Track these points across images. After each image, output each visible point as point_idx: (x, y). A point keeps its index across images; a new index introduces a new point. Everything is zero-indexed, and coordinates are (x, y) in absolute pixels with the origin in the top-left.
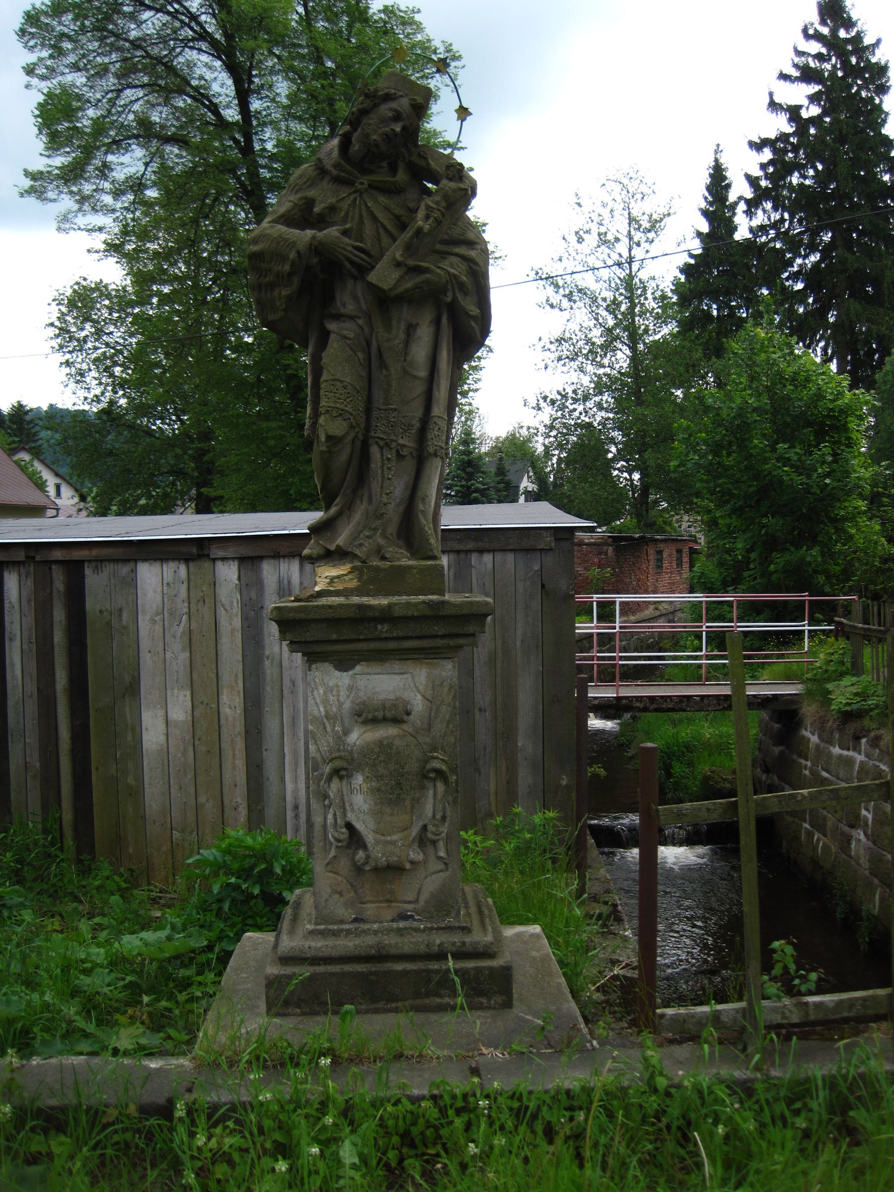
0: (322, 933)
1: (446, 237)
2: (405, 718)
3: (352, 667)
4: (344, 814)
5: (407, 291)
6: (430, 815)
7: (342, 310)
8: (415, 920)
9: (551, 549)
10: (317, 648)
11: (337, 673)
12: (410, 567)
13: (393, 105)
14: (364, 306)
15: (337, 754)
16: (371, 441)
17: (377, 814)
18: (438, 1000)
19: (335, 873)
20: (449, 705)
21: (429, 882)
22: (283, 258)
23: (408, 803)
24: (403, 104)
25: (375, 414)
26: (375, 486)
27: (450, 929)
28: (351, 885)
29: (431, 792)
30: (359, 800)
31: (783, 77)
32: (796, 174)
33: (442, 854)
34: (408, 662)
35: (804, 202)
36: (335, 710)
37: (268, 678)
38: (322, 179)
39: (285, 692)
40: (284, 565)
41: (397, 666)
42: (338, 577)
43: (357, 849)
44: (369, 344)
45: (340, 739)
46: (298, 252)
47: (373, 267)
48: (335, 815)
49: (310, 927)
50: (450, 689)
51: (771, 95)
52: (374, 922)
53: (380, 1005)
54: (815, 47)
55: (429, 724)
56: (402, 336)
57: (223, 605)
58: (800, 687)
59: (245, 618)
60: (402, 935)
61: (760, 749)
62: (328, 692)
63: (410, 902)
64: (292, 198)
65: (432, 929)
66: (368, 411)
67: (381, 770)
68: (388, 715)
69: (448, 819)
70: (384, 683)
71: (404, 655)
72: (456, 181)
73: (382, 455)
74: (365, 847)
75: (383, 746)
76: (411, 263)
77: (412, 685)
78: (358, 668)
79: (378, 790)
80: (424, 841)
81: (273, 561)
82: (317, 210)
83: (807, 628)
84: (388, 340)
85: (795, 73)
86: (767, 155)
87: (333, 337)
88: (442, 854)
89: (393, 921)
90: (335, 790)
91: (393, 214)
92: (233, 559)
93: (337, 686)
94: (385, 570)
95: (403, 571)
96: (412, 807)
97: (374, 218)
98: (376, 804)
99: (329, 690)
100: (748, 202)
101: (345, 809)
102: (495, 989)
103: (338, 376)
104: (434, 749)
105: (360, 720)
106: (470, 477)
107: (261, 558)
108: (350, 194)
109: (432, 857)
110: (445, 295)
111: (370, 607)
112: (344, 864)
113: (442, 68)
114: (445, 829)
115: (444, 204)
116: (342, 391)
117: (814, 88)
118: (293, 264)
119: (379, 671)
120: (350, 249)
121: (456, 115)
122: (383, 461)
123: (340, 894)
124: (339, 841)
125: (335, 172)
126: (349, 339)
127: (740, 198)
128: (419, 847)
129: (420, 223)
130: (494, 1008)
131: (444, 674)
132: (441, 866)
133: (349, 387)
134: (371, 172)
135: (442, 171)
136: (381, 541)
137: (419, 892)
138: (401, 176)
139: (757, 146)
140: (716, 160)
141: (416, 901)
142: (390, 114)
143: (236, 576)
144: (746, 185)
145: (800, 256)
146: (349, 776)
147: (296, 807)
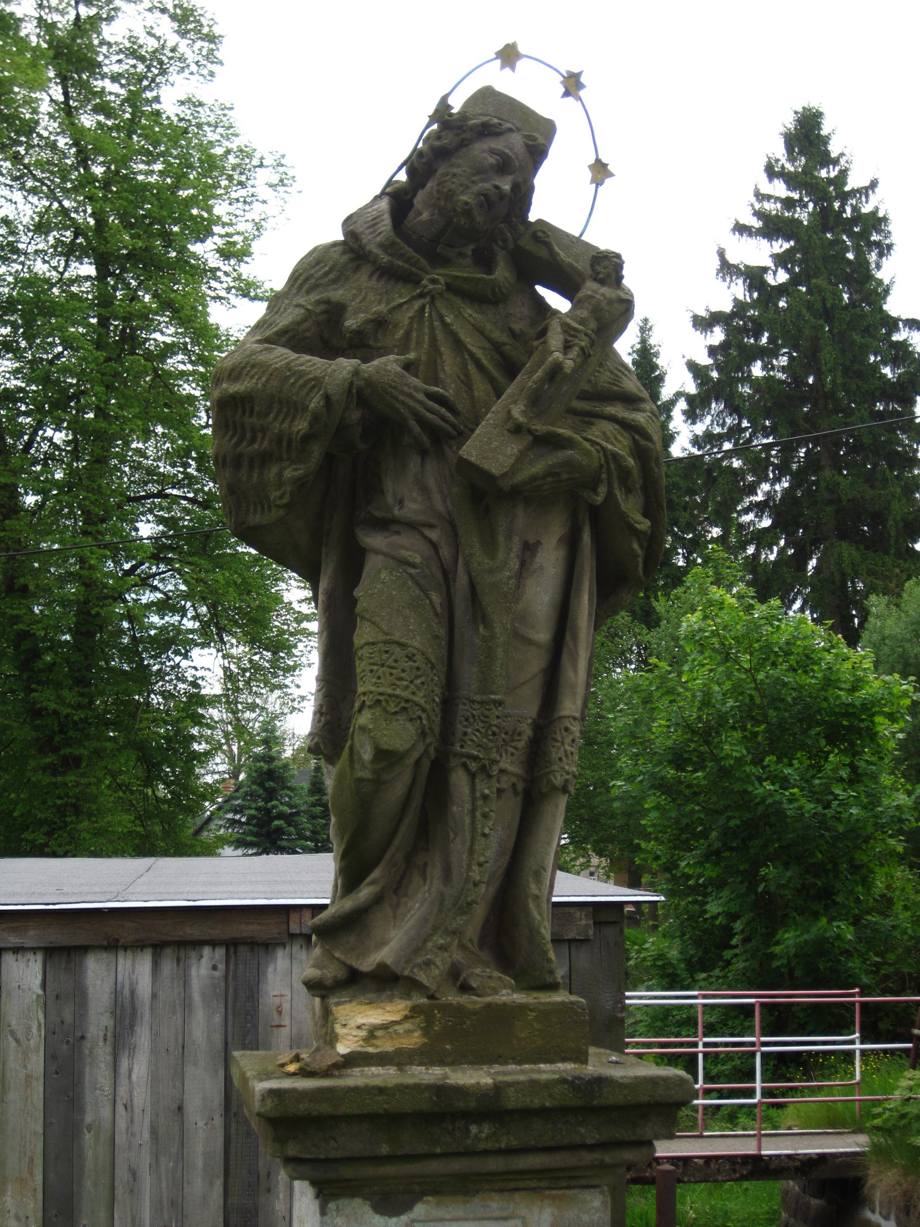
1: (587, 387)
3: (406, 1207)
5: (534, 478)
7: (396, 512)
9: (586, 941)
10: (346, 1172)
11: (378, 1220)
12: (523, 1008)
13: (498, 144)
14: (439, 505)
16: (454, 762)
22: (294, 408)
24: (515, 143)
25: (462, 709)
26: (459, 847)
31: (741, 229)
32: (759, 364)
34: (517, 1196)
35: (774, 404)
37: (89, 1165)
38: (357, 269)
39: (119, 1191)
40: (124, 962)
41: (495, 1204)
42: (385, 1027)
44: (448, 576)
46: (327, 398)
47: (473, 431)
51: (721, 254)
54: (780, 189)
56: (515, 564)
57: (12, 1033)
58: (863, 1139)
59: (51, 1056)
64: (302, 301)
66: (448, 704)
72: (610, 286)
73: (473, 790)
76: (540, 428)
78: (420, 1209)
81: (105, 955)
82: (351, 323)
83: (858, 1046)
84: (491, 571)
85: (756, 223)
86: (718, 336)
87: (373, 563)
91: (489, 340)
92: (34, 950)
94: (475, 1013)
95: (505, 1015)
97: (458, 345)
100: (690, 399)
103: (397, 636)
106: (271, 795)
107: (84, 949)
108: (414, 298)
110: (595, 490)
111: (460, 1091)
113: (572, 90)
115: (593, 325)
116: (408, 665)
117: (781, 246)
118: (316, 418)
119: (460, 1214)
120: (421, 397)
121: (589, 175)
122: (474, 800)
125: (385, 258)
126: (413, 566)
127: (679, 395)
129: (558, 355)
133: (418, 657)
134: (445, 262)
135: (583, 266)
136: (458, 956)
138: (502, 273)
139: (703, 323)
140: (643, 341)
142: (492, 160)
143: (38, 981)
144: (689, 377)
145: (766, 480)
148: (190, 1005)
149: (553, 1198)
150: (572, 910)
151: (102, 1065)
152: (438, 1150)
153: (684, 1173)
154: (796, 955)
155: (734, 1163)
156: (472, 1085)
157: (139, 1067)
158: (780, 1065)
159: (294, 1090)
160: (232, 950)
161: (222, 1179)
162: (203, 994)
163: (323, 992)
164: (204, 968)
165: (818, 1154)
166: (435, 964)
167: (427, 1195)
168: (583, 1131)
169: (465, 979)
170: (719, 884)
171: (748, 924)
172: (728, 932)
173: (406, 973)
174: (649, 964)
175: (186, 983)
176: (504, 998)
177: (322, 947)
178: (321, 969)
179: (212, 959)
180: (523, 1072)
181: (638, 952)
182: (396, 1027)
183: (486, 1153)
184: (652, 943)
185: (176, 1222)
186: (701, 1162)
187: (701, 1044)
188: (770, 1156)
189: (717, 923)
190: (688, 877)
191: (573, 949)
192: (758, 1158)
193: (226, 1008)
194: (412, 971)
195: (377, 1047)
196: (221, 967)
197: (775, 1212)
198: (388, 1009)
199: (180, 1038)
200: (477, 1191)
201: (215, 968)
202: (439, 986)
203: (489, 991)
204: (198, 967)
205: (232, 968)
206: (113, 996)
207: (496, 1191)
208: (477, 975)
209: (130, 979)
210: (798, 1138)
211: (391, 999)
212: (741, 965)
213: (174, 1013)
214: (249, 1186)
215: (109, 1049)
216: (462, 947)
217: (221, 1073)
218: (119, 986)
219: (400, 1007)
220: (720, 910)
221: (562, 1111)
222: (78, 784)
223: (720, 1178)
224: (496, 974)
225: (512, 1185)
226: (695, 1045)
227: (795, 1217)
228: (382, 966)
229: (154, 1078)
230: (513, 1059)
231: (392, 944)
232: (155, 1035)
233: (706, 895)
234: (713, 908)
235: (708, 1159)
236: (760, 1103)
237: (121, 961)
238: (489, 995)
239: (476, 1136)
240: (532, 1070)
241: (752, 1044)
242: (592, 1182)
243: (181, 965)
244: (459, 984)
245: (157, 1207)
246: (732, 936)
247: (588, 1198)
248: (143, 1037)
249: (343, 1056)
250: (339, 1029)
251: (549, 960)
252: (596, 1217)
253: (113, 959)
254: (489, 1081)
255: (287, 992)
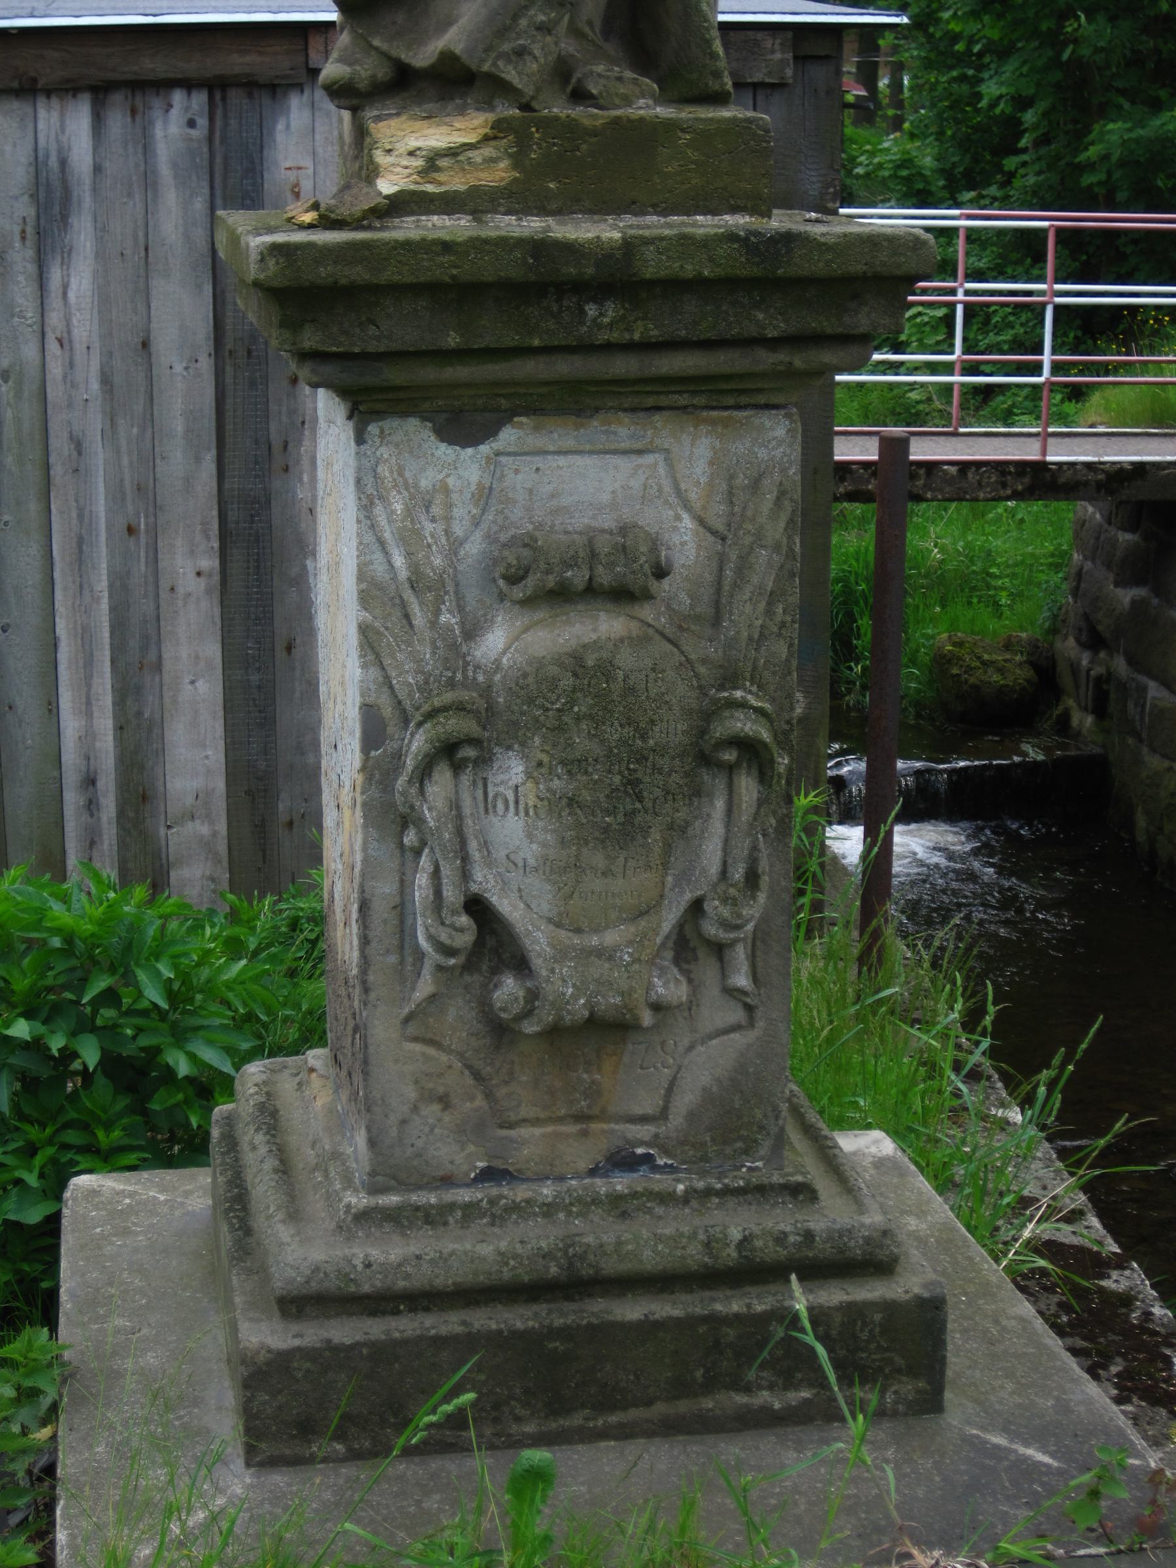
0: (394, 1218)
2: (654, 585)
3: (488, 432)
4: (465, 875)
6: (714, 870)
8: (656, 1168)
10: (395, 375)
11: (444, 451)
12: (670, 126)
15: (449, 697)
17: (565, 871)
18: (741, 1399)
19: (430, 1042)
20: (777, 548)
21: (702, 1061)
23: (655, 836)
27: (759, 1192)
28: (477, 1076)
29: (720, 804)
30: (513, 832)
33: (742, 980)
36: (438, 561)
39: (57, 471)
40: (48, 115)
41: (624, 430)
42: (452, 152)
43: (495, 971)
45: (456, 648)
48: (436, 874)
49: (358, 1200)
50: (778, 502)
52: (542, 1178)
53: (576, 1420)
55: (717, 604)
60: (624, 1215)
61: (1075, 592)
62: (360, 502)
63: (644, 1119)
65: (708, 1192)
67: (582, 742)
68: (604, 577)
69: (765, 880)
70: (591, 479)
71: (648, 397)
74: (521, 965)
75: (587, 670)
77: (668, 488)
78: (508, 436)
79: (572, 802)
80: (689, 945)
88: (742, 980)
89: (593, 1172)
90: (440, 804)
93: (446, 490)
94: (595, 133)
95: (644, 137)
96: (668, 849)
98: (563, 842)
99: (421, 502)
101: (465, 859)
102: (900, 1361)
104: (730, 679)
105: (518, 593)
109: (712, 991)
111: (569, 249)
112: (458, 1017)
114: (754, 910)
119: (570, 443)
123: (445, 1101)
124: (449, 951)
128: (677, 961)
130: (895, 1414)
131: (762, 454)
132: (737, 1015)
136: (569, 46)
137: (670, 1090)
141: (663, 1115)
146: (484, 761)
147: (90, 781)
148: (155, 183)
149: (713, 422)
150: (760, 35)
151: (21, 278)
152: (536, 342)
153: (927, 487)
154: (1122, 164)
155: (1004, 473)
156: (590, 241)
157: (79, 281)
158: (1085, 328)
159: (311, 245)
160: (218, 96)
161: (214, 452)
162: (175, 166)
163: (355, 102)
164: (175, 125)
165: (1132, 463)
166: (531, 53)
167: (520, 415)
168: (761, 316)
169: (579, 81)
170: (1003, 52)
171: (1045, 114)
172: (1013, 127)
173: (486, 67)
174: (886, 173)
175: (147, 147)
176: (642, 112)
177: (353, 31)
178: (350, 65)
179: (187, 109)
180: (669, 226)
181: (872, 154)
182: (470, 154)
183: (609, 347)
184: (891, 145)
185: (146, 517)
186: (953, 470)
187: (960, 292)
188: (1060, 464)
189: (998, 111)
190: (955, 38)
191: (759, 98)
192: (1039, 468)
193: (212, 188)
194: (494, 64)
195: (440, 184)
196: (202, 122)
197: (1063, 554)
198: (457, 125)
199: (141, 234)
200: (597, 410)
201: (191, 124)
202: (538, 90)
203: (617, 101)
204: (166, 122)
205: (219, 123)
206: (32, 169)
207: (625, 410)
208: (600, 76)
209: (58, 141)
210: (1104, 439)
211: (461, 111)
212: (1032, 180)
213: (130, 195)
214: (256, 463)
215: (30, 253)
216: (575, 32)
217: (208, 289)
218: (41, 154)
219: (476, 122)
220: (1004, 90)
221: (729, 285)
222: (187, 1194)
223: (981, 495)
224: (629, 74)
225: (650, 401)
226: (953, 292)
227: (1093, 560)
228: (447, 58)
229: (103, 299)
230: (654, 206)
231: (463, 21)
232: (101, 231)
233: (980, 68)
234: (991, 89)
235: (964, 466)
236: (1052, 386)
237: (42, 113)
238: (618, 107)
239: (594, 320)
240: (683, 224)
241: (1041, 293)
242: (775, 400)
243: (138, 118)
244: (569, 89)
245: (117, 496)
246: (1019, 135)
247: (768, 424)
248: (82, 233)
249: (387, 197)
250: (380, 158)
251: (714, 56)
252: (778, 453)
253: (29, 110)
254: (617, 235)
255: (307, 163)
